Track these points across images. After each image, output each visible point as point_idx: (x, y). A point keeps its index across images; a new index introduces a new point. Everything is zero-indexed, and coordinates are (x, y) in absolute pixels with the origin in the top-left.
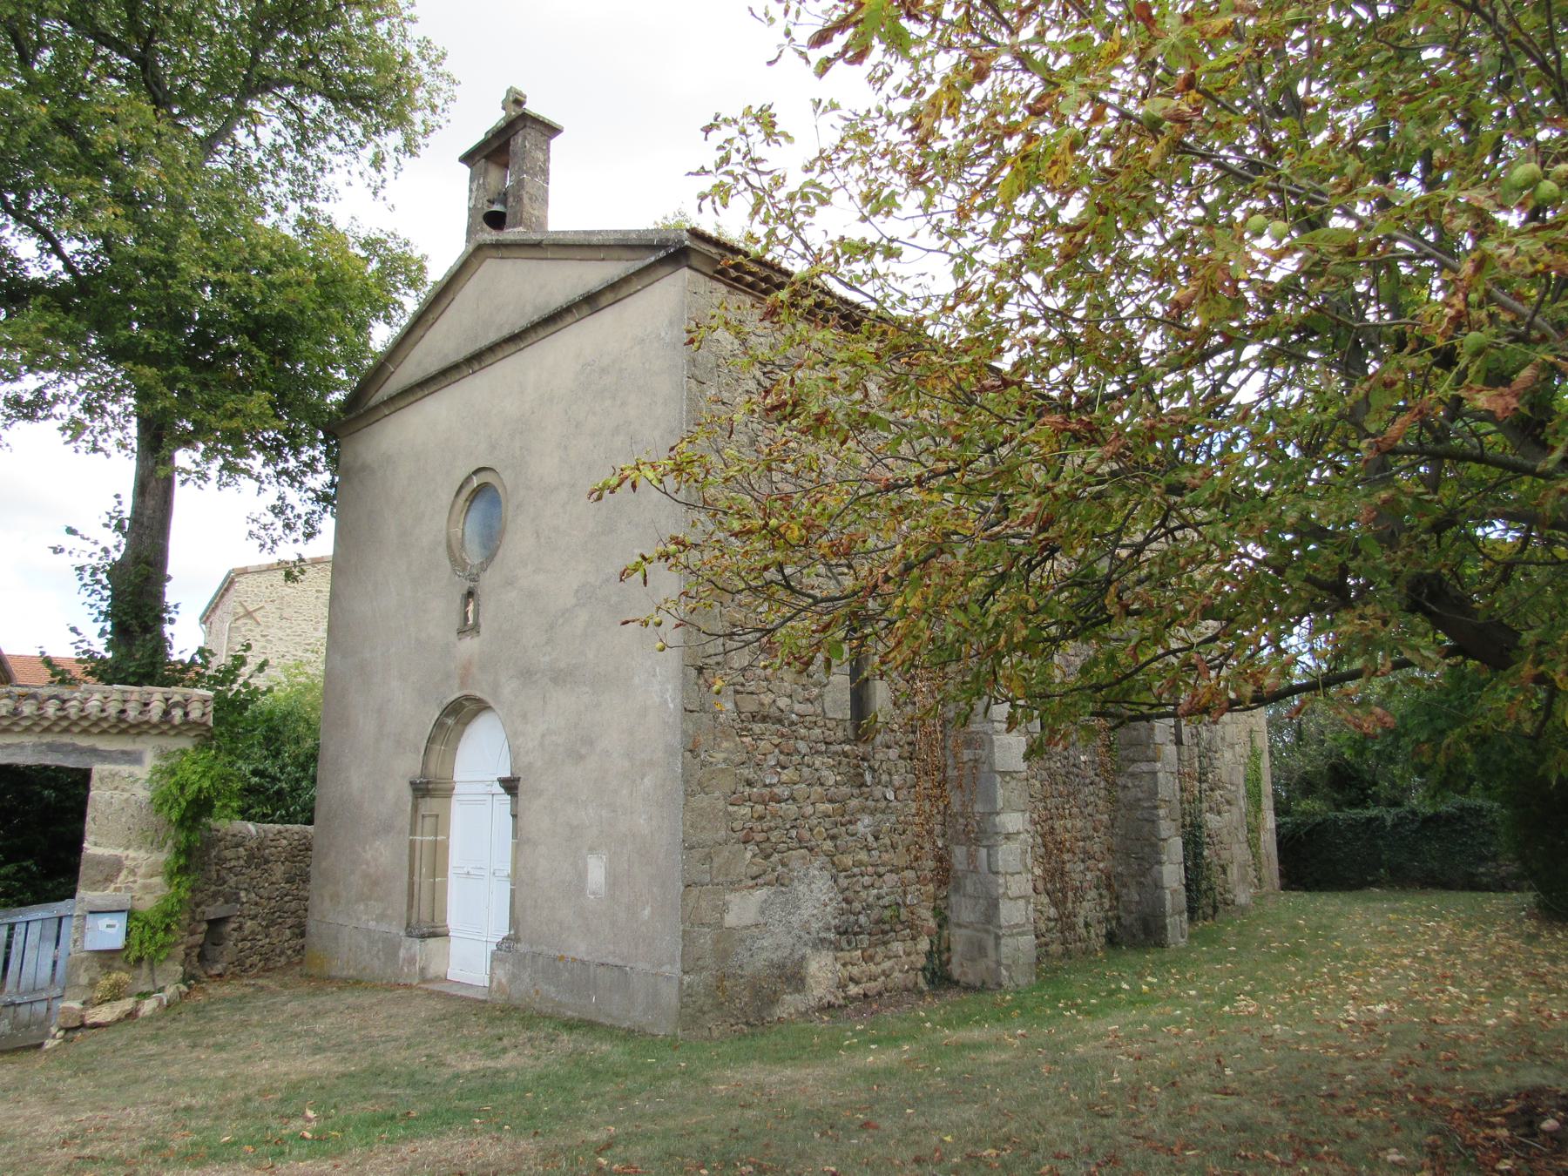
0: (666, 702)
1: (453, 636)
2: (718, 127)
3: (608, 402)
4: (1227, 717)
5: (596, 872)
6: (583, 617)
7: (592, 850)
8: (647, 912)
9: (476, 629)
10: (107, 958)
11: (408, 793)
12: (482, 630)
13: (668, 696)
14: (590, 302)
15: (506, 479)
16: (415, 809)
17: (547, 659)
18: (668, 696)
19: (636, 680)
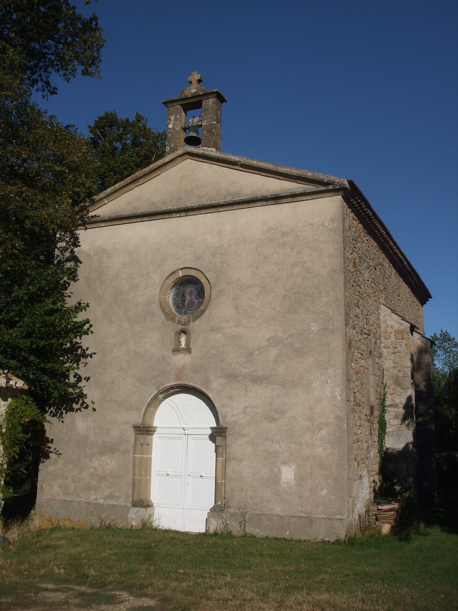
0: (335, 396)
1: (168, 353)
2: (88, 334)
3: (288, 250)
4: (233, 461)
5: (288, 474)
6: (273, 353)
7: (284, 463)
8: (324, 492)
9: (188, 350)
10: (19, 422)
11: (131, 433)
12: (193, 350)
13: (337, 393)
14: (276, 199)
15: (209, 277)
16: (136, 440)
17: (247, 370)
18: (337, 393)
19: (314, 385)
